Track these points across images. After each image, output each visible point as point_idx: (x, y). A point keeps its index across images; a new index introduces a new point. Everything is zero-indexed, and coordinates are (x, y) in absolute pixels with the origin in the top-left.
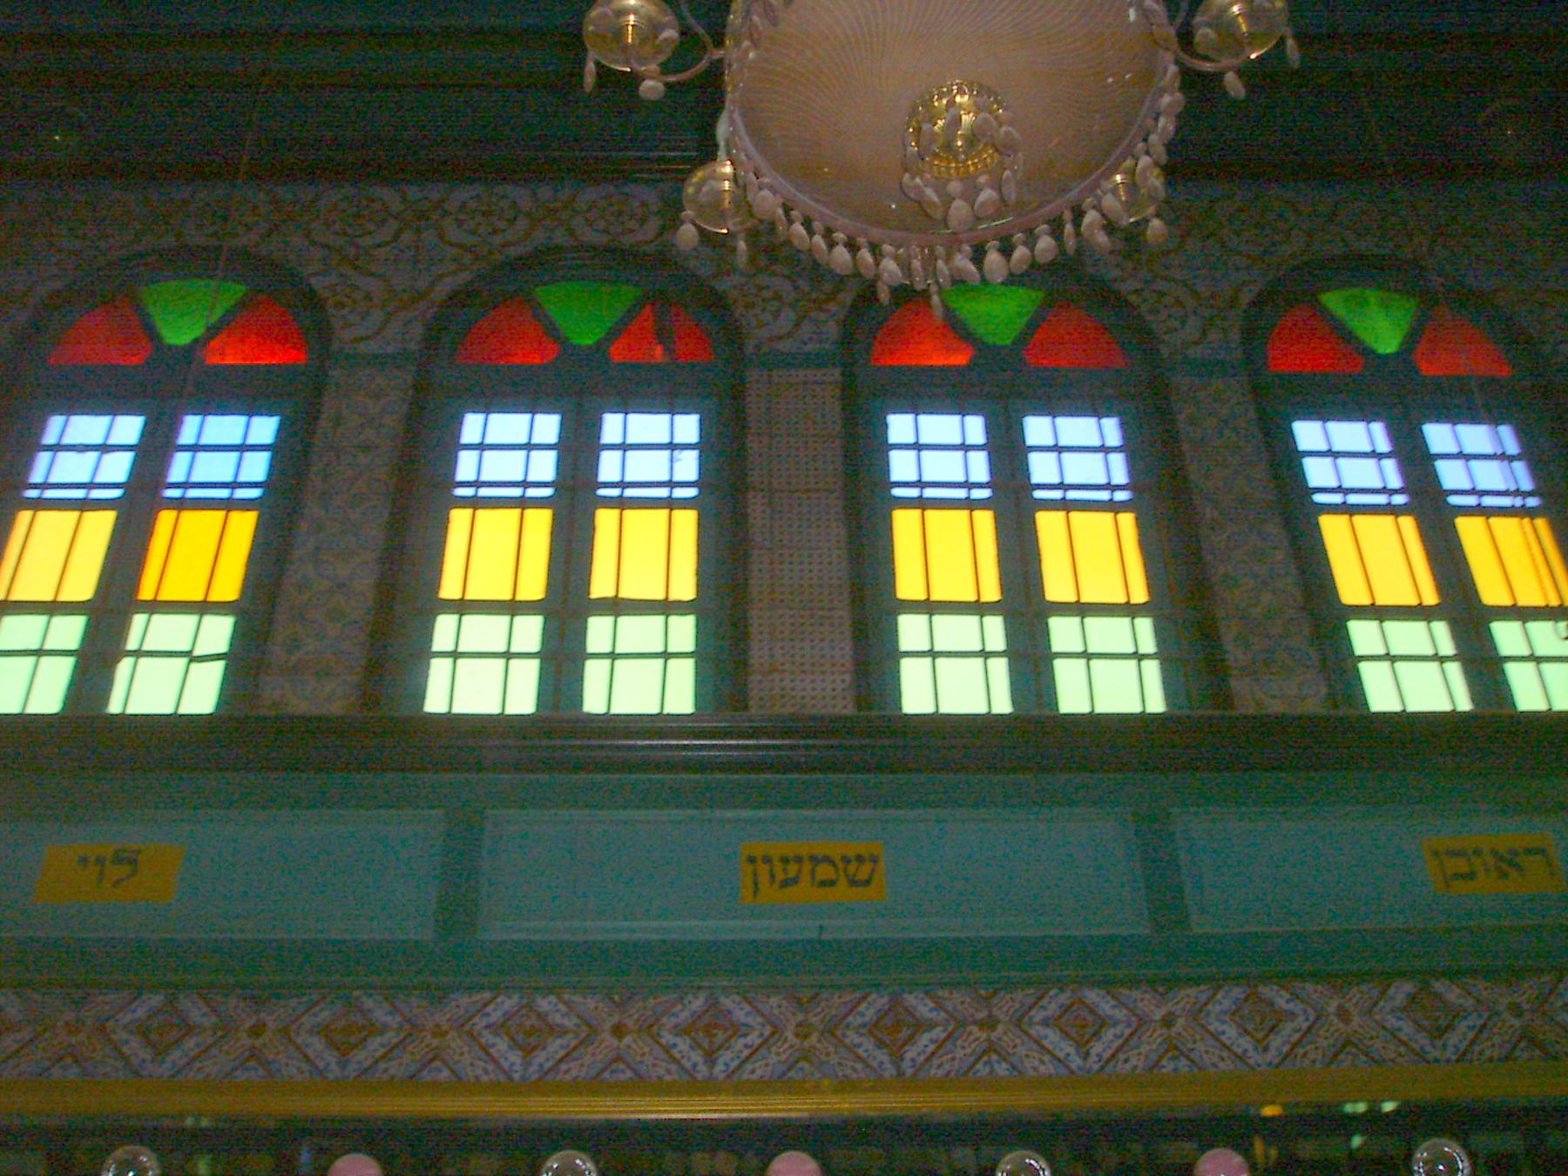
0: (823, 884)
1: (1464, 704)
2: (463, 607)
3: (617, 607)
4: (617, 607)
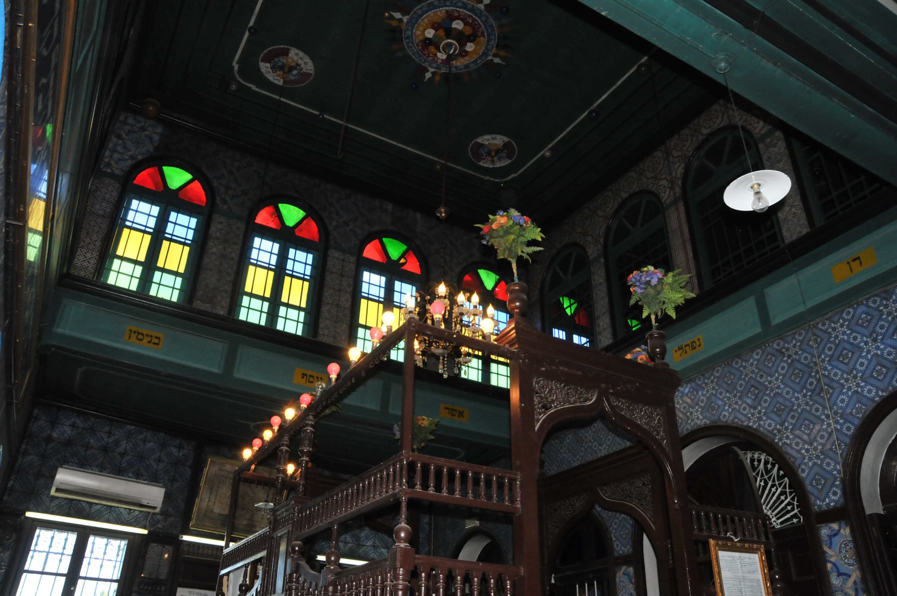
0: (139, 339)
1: (480, 380)
2: (122, 258)
3: (163, 270)
4: (163, 270)
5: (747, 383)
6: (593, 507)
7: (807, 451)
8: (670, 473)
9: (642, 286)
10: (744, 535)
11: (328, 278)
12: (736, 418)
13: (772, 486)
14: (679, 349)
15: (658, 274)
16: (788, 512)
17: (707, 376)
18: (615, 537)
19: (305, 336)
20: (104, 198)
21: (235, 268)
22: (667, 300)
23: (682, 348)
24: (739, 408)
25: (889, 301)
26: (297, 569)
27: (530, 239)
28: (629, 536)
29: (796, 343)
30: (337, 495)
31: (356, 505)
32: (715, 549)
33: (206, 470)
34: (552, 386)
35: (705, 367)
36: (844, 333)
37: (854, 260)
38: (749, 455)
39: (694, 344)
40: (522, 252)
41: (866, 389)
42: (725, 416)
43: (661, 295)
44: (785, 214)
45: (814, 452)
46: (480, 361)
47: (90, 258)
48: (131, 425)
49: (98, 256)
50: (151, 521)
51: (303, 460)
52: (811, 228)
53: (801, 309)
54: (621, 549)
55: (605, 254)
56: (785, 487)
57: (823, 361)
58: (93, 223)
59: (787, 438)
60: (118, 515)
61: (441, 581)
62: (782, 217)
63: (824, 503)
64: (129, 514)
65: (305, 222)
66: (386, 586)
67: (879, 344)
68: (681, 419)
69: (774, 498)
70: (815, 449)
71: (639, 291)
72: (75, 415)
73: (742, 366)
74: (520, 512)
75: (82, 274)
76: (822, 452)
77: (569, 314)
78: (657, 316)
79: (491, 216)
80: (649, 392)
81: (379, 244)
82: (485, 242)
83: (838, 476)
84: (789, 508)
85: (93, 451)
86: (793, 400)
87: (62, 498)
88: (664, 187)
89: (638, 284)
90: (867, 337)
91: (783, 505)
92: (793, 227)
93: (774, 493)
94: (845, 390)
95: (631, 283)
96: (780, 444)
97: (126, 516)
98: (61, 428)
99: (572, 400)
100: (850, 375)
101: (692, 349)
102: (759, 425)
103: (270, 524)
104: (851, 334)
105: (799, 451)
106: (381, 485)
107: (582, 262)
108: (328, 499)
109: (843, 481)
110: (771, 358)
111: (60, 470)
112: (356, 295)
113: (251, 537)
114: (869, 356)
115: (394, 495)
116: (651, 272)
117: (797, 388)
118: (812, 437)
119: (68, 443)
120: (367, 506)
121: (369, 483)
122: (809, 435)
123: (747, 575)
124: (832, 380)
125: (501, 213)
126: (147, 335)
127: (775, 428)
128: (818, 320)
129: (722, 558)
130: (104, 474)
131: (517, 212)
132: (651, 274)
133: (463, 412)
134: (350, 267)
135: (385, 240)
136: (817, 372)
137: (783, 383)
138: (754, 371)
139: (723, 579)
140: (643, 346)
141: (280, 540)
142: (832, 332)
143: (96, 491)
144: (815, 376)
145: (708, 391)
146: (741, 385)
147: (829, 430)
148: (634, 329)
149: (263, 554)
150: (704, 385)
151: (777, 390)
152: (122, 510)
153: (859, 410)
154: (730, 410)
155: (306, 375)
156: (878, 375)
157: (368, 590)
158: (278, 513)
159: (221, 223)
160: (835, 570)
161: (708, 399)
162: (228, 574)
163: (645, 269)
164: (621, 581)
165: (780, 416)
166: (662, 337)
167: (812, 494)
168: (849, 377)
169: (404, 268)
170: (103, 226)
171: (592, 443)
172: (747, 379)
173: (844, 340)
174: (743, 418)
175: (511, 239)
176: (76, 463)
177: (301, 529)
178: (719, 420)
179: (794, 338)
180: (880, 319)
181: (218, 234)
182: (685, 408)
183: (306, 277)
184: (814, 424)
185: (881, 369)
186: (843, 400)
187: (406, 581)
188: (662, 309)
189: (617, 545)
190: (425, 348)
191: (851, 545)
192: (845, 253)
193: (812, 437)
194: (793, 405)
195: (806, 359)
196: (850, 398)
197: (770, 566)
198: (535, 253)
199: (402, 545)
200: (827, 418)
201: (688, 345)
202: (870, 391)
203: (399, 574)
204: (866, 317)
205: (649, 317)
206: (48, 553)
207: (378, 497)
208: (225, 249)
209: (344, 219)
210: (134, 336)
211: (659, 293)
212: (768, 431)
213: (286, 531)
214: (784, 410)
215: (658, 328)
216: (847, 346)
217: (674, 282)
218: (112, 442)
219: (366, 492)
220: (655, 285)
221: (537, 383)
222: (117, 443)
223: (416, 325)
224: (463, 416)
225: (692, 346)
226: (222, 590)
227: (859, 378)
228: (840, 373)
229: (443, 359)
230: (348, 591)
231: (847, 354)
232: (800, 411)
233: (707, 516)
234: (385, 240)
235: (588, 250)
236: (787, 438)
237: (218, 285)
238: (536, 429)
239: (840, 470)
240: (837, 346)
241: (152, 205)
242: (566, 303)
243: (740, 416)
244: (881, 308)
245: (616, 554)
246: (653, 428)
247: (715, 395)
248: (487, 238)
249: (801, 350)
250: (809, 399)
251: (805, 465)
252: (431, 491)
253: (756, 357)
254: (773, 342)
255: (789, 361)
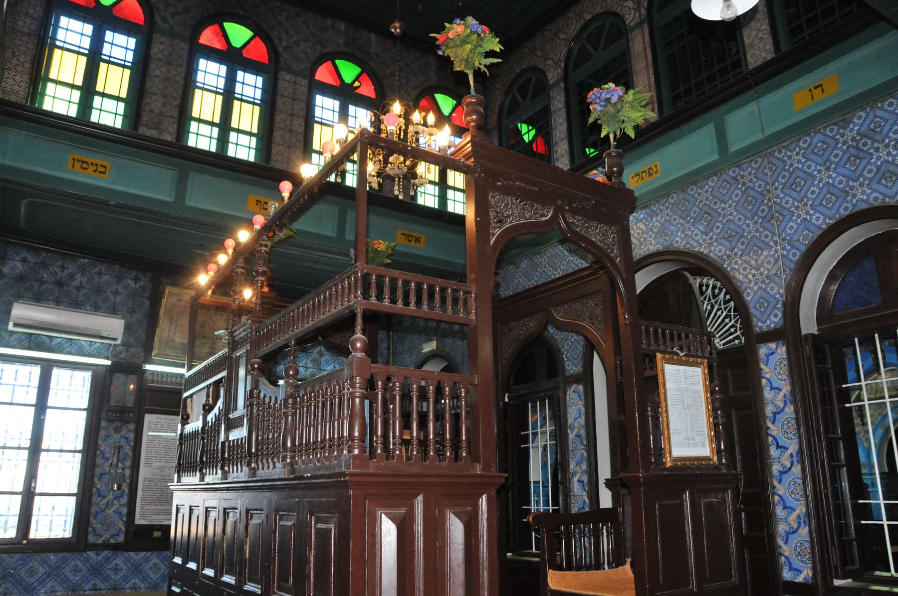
1: (437, 207)
5: (701, 209)
6: (545, 329)
7: (754, 275)
8: (622, 289)
9: (602, 103)
10: (689, 350)
11: (280, 102)
12: (688, 243)
13: (718, 310)
14: (636, 176)
15: (619, 91)
16: (732, 334)
17: (662, 202)
18: (566, 357)
19: (258, 162)
20: (27, 14)
21: (180, 91)
22: (627, 119)
23: (639, 175)
24: (692, 234)
25: (846, 130)
26: (255, 385)
27: (488, 50)
28: (581, 356)
29: (752, 170)
30: (294, 311)
31: (312, 319)
32: (661, 362)
33: (164, 301)
34: (508, 201)
35: (661, 194)
36: (799, 162)
37: (816, 88)
38: (698, 280)
39: (651, 170)
40: (480, 64)
41: (814, 217)
42: (677, 242)
43: (621, 114)
44: (751, 38)
45: (760, 277)
46: (437, 188)
47: (19, 82)
48: (85, 258)
49: (29, 79)
50: (113, 353)
51: (258, 281)
52: (776, 54)
53: (759, 136)
54: (572, 369)
55: (566, 78)
56: (730, 311)
57: (776, 189)
58: (18, 42)
59: (736, 263)
60: (79, 347)
61: (398, 389)
62: (748, 43)
63: (765, 325)
64: (91, 346)
65: (252, 43)
66: (343, 395)
67: (831, 173)
68: (635, 244)
69: (719, 321)
70: (762, 274)
71: (599, 108)
72: (25, 249)
73: (697, 192)
74: (475, 324)
75: (13, 99)
76: (767, 277)
77: (527, 141)
78: (615, 135)
79: (447, 25)
80: (605, 210)
81: (332, 66)
82: (441, 53)
83: (780, 299)
84: (732, 330)
85: (48, 285)
86: (744, 226)
87: (21, 333)
88: (629, 8)
89: (598, 101)
90: (820, 165)
91: (727, 327)
92: (758, 52)
93: (720, 316)
94: (794, 218)
95: (591, 100)
96: (729, 269)
97: (88, 348)
98: (11, 264)
99: (528, 216)
100: (801, 203)
101: (649, 176)
102: (710, 251)
103: (229, 345)
104: (806, 162)
105: (746, 276)
106: (337, 298)
107: (542, 88)
108: (284, 316)
109: (784, 304)
110: (726, 185)
111: (15, 305)
112: (309, 120)
113: (211, 359)
114: (821, 185)
115: (349, 307)
116: (611, 89)
117: (749, 215)
118: (759, 262)
119: (21, 278)
120: (323, 319)
121: (325, 298)
122: (756, 260)
123: (690, 386)
124: (783, 207)
125: (458, 21)
126: (92, 164)
127: (725, 254)
128: (775, 148)
129: (667, 371)
130: (62, 308)
131: (474, 20)
132: (612, 91)
133: (420, 238)
134: (302, 90)
135: (338, 62)
136: (769, 200)
137: (736, 210)
138: (708, 197)
139: (668, 390)
140: (600, 169)
141: (239, 359)
142: (788, 161)
143: (55, 325)
144: (768, 203)
145: (662, 218)
146: (695, 212)
147: (776, 256)
148: (591, 156)
149: (224, 374)
150: (658, 211)
151: (729, 217)
152: (83, 343)
153: (805, 241)
154: (683, 236)
155: (260, 202)
156: (827, 204)
157: (326, 400)
158: (235, 334)
159: (162, 43)
160: (769, 385)
161: (662, 225)
162: (191, 396)
163: (606, 86)
164: (570, 399)
165: (730, 242)
166: (620, 156)
167: (755, 316)
168: (799, 204)
169: (359, 91)
170: (31, 46)
171: (547, 268)
172: (701, 205)
173: (799, 169)
174: (695, 244)
175: (468, 50)
176: (32, 298)
177: (259, 347)
178: (672, 245)
179: (750, 166)
180: (835, 148)
181: (160, 55)
182: (638, 234)
183: (256, 101)
184: (762, 250)
185: (831, 197)
186: (791, 227)
187: (363, 389)
188: (621, 129)
189: (569, 365)
190: (379, 169)
191: (785, 362)
192: (808, 80)
193: (759, 262)
194: (744, 231)
195: (760, 186)
196: (799, 225)
197: (712, 380)
198: (492, 64)
199: (359, 355)
200: (775, 244)
201: (645, 171)
202: (818, 219)
203: (356, 383)
204: (822, 146)
205: (607, 136)
206: (14, 385)
207: (333, 311)
208: (169, 71)
209: (294, 39)
210: (78, 165)
211: (619, 111)
212: (718, 256)
213: (244, 350)
214: (735, 236)
215: (616, 147)
216: (801, 174)
217: (635, 100)
218: (67, 275)
219: (322, 306)
220: (615, 103)
221: (494, 198)
222: (71, 277)
223: (368, 136)
224: (419, 242)
225: (649, 172)
226: (186, 411)
227: (809, 206)
228: (791, 201)
229: (399, 181)
230: (307, 402)
231: (800, 182)
232: (750, 237)
233: (656, 331)
234: (338, 62)
235: (548, 74)
236: (736, 263)
237: (163, 110)
238: (492, 243)
239: (783, 294)
240: (791, 174)
241: (118, 101)
242: (524, 128)
243: (693, 242)
244: (837, 137)
245: (567, 374)
246: (608, 245)
247: (669, 221)
248: (443, 48)
249: (755, 177)
250: (760, 225)
251: (751, 289)
252: (386, 302)
253: (711, 184)
254: (729, 170)
255: (744, 188)
